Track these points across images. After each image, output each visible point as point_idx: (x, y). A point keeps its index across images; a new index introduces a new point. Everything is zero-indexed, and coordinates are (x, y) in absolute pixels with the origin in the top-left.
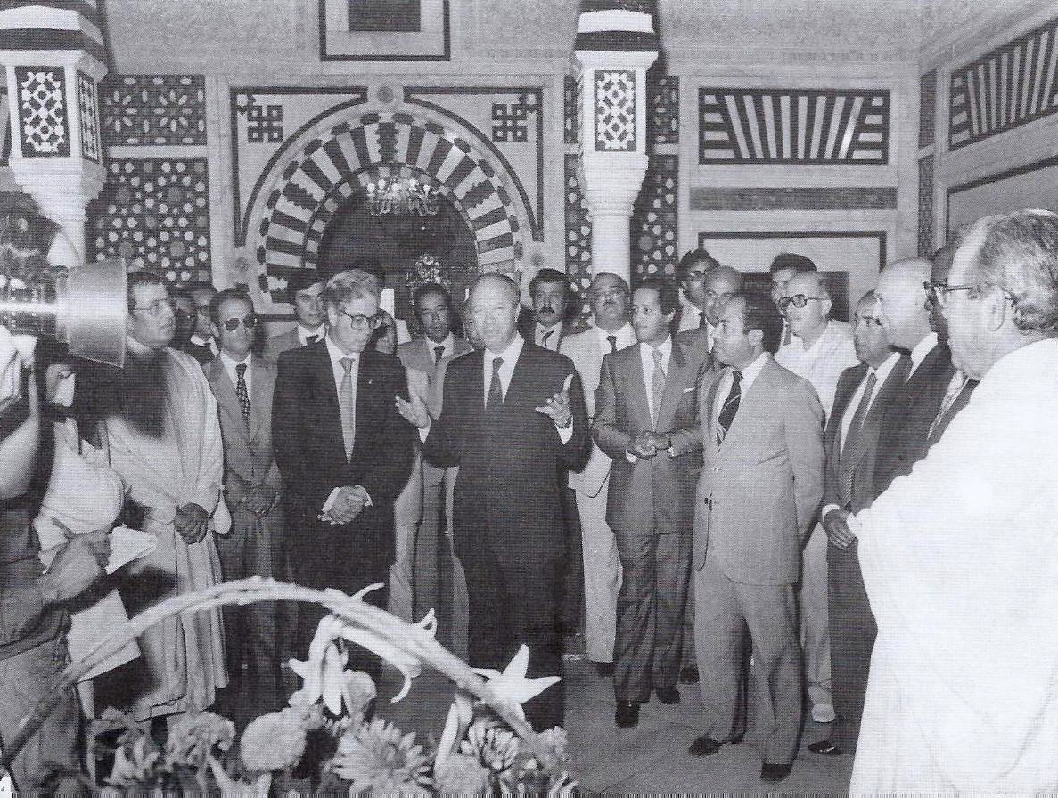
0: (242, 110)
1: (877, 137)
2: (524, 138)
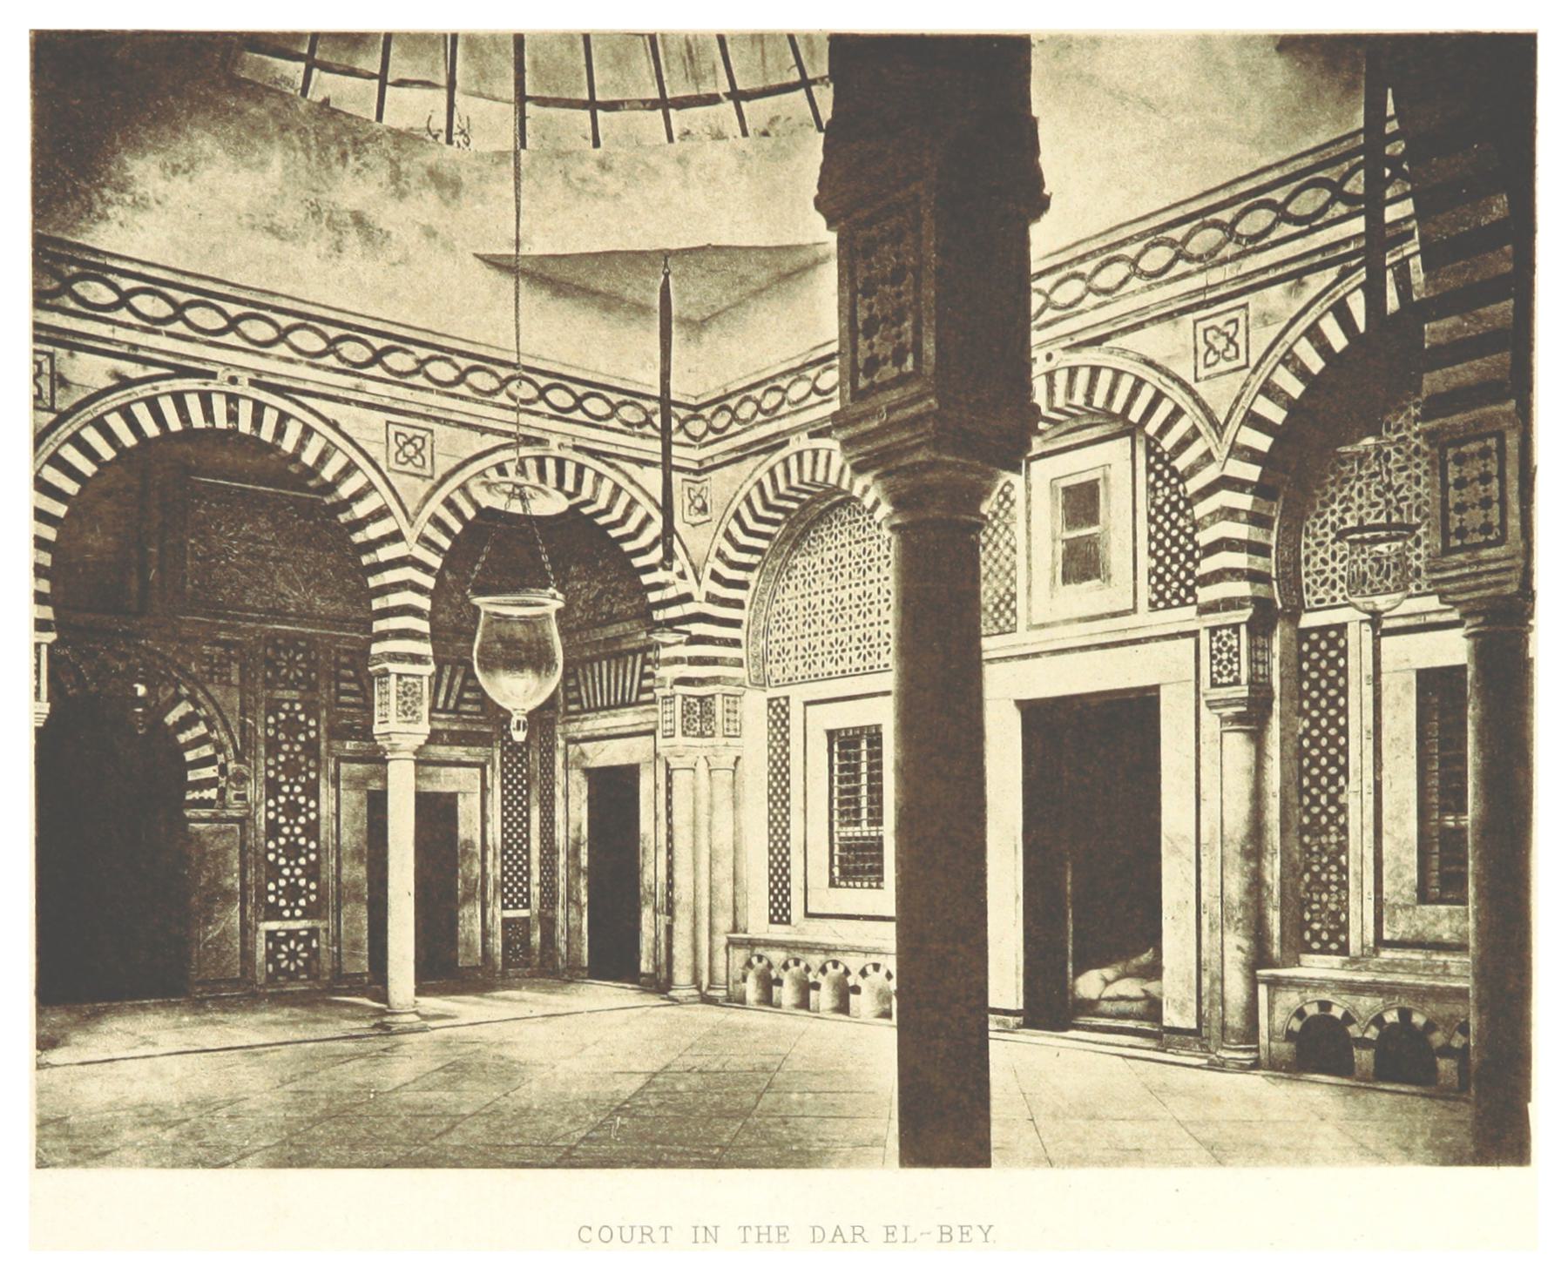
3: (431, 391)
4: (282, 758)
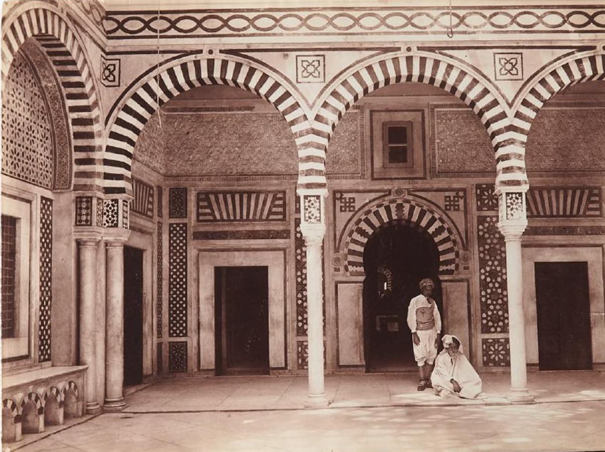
0: (338, 199)
1: (281, 210)
3: (367, 34)
4: (487, 247)
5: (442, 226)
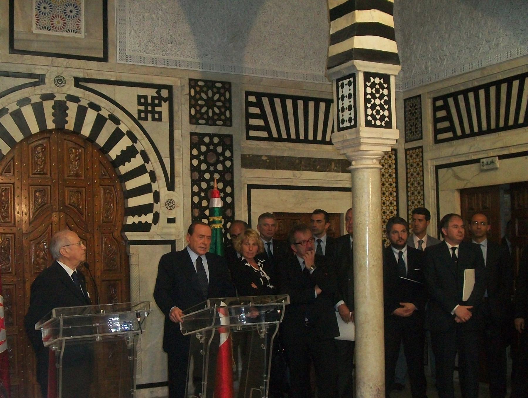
2: (160, 119)
5: (133, 146)
